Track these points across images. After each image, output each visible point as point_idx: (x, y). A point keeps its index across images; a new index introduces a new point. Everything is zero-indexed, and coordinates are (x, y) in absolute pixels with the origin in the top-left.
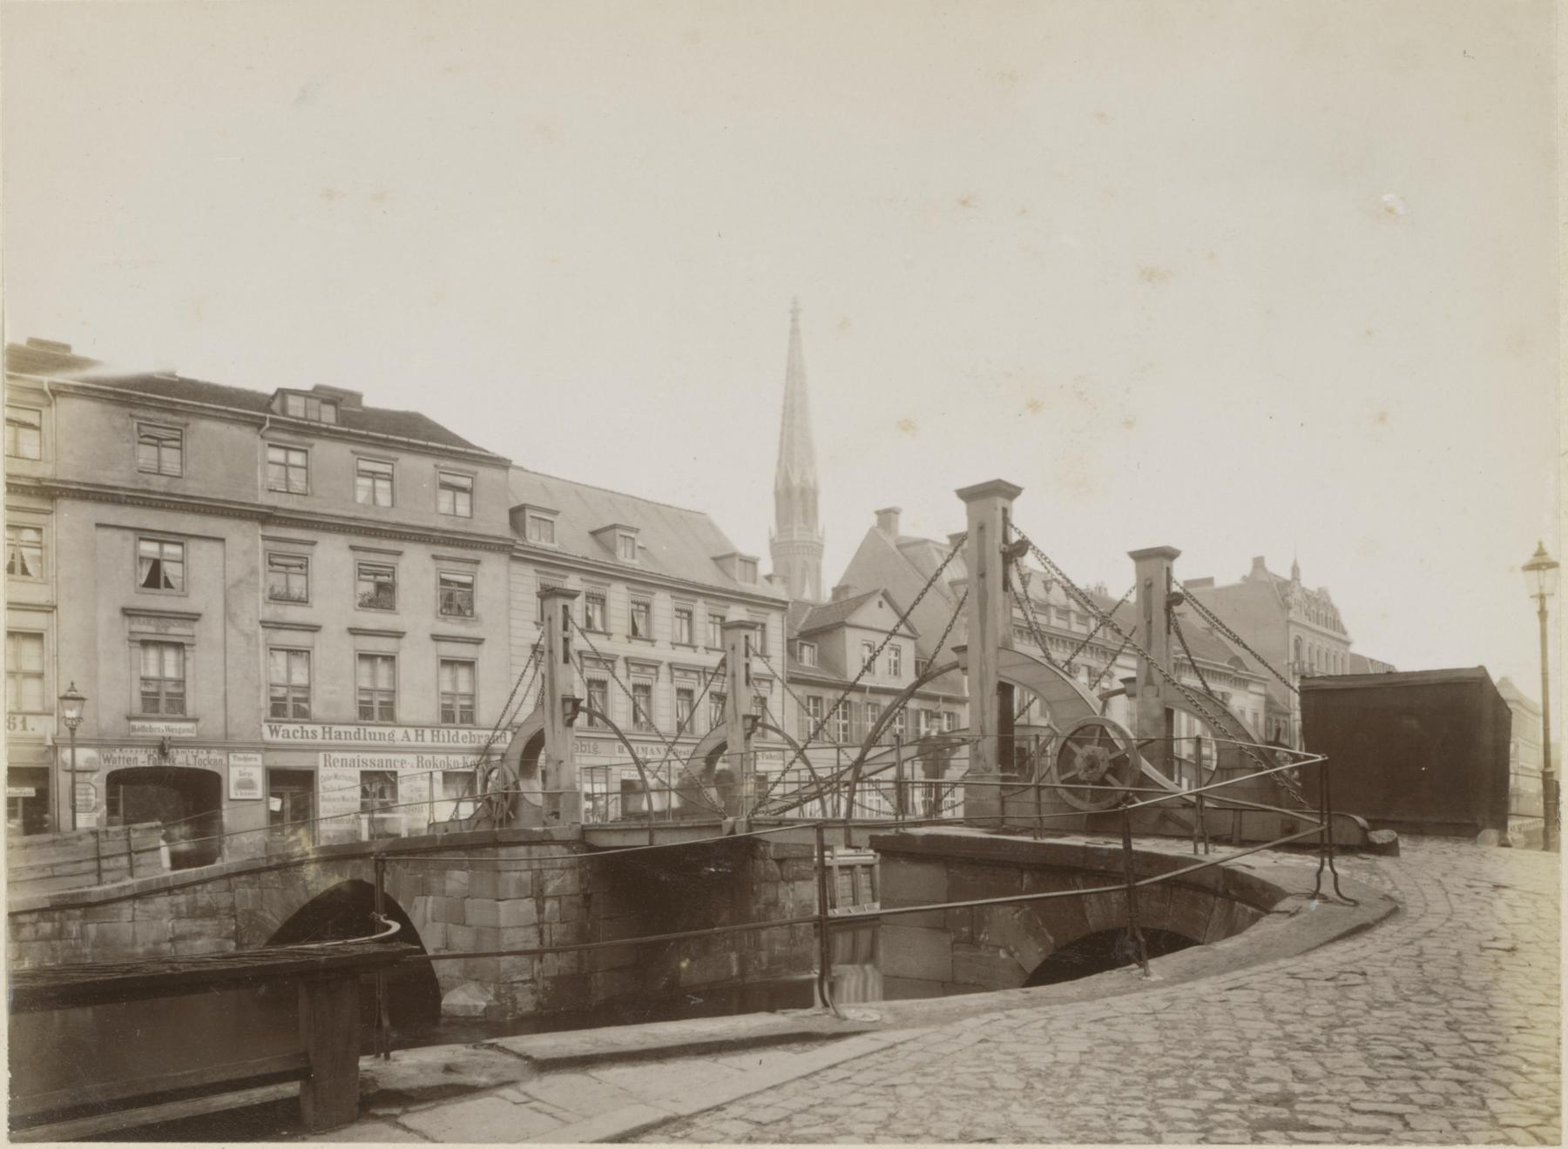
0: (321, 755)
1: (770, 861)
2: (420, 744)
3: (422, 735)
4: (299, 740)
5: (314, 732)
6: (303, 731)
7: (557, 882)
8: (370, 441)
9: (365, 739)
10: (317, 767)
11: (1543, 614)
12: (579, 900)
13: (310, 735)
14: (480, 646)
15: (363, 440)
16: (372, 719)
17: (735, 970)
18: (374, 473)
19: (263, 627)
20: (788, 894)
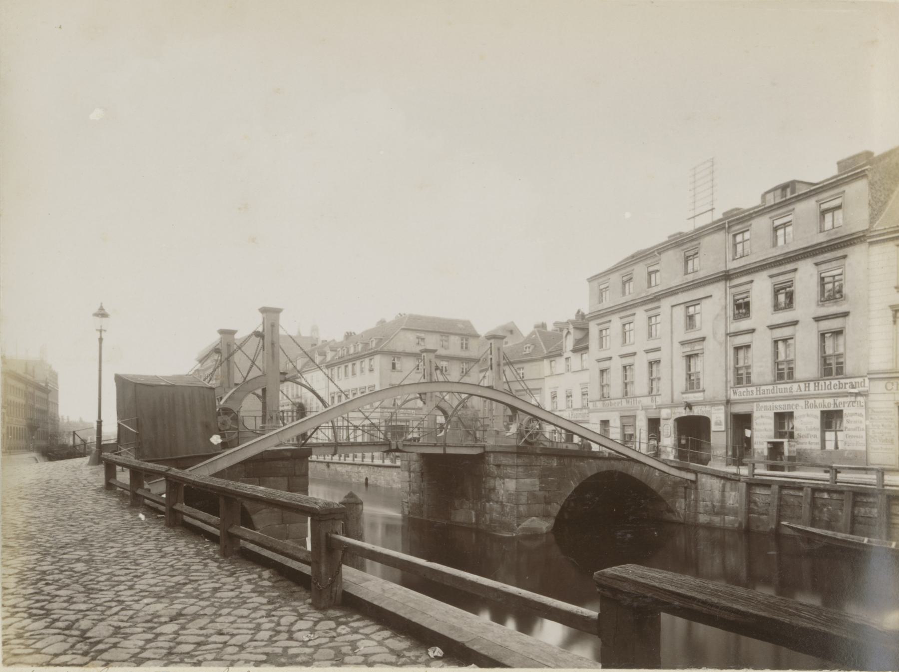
0: (755, 404)
1: (491, 466)
2: (807, 392)
3: (809, 387)
4: (745, 397)
5: (752, 391)
6: (839, 384)
7: (414, 466)
8: (767, 210)
9: (777, 393)
10: (753, 412)
11: (101, 340)
12: (419, 474)
13: (751, 393)
14: (847, 318)
15: (772, 209)
16: (742, 384)
17: (474, 520)
18: (785, 224)
19: (682, 345)
20: (501, 485)
